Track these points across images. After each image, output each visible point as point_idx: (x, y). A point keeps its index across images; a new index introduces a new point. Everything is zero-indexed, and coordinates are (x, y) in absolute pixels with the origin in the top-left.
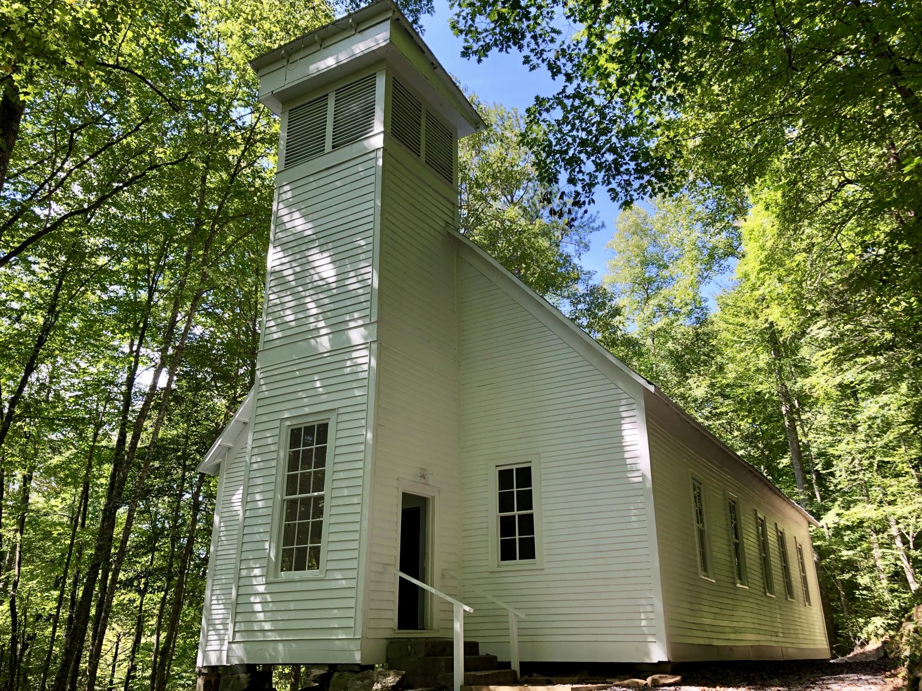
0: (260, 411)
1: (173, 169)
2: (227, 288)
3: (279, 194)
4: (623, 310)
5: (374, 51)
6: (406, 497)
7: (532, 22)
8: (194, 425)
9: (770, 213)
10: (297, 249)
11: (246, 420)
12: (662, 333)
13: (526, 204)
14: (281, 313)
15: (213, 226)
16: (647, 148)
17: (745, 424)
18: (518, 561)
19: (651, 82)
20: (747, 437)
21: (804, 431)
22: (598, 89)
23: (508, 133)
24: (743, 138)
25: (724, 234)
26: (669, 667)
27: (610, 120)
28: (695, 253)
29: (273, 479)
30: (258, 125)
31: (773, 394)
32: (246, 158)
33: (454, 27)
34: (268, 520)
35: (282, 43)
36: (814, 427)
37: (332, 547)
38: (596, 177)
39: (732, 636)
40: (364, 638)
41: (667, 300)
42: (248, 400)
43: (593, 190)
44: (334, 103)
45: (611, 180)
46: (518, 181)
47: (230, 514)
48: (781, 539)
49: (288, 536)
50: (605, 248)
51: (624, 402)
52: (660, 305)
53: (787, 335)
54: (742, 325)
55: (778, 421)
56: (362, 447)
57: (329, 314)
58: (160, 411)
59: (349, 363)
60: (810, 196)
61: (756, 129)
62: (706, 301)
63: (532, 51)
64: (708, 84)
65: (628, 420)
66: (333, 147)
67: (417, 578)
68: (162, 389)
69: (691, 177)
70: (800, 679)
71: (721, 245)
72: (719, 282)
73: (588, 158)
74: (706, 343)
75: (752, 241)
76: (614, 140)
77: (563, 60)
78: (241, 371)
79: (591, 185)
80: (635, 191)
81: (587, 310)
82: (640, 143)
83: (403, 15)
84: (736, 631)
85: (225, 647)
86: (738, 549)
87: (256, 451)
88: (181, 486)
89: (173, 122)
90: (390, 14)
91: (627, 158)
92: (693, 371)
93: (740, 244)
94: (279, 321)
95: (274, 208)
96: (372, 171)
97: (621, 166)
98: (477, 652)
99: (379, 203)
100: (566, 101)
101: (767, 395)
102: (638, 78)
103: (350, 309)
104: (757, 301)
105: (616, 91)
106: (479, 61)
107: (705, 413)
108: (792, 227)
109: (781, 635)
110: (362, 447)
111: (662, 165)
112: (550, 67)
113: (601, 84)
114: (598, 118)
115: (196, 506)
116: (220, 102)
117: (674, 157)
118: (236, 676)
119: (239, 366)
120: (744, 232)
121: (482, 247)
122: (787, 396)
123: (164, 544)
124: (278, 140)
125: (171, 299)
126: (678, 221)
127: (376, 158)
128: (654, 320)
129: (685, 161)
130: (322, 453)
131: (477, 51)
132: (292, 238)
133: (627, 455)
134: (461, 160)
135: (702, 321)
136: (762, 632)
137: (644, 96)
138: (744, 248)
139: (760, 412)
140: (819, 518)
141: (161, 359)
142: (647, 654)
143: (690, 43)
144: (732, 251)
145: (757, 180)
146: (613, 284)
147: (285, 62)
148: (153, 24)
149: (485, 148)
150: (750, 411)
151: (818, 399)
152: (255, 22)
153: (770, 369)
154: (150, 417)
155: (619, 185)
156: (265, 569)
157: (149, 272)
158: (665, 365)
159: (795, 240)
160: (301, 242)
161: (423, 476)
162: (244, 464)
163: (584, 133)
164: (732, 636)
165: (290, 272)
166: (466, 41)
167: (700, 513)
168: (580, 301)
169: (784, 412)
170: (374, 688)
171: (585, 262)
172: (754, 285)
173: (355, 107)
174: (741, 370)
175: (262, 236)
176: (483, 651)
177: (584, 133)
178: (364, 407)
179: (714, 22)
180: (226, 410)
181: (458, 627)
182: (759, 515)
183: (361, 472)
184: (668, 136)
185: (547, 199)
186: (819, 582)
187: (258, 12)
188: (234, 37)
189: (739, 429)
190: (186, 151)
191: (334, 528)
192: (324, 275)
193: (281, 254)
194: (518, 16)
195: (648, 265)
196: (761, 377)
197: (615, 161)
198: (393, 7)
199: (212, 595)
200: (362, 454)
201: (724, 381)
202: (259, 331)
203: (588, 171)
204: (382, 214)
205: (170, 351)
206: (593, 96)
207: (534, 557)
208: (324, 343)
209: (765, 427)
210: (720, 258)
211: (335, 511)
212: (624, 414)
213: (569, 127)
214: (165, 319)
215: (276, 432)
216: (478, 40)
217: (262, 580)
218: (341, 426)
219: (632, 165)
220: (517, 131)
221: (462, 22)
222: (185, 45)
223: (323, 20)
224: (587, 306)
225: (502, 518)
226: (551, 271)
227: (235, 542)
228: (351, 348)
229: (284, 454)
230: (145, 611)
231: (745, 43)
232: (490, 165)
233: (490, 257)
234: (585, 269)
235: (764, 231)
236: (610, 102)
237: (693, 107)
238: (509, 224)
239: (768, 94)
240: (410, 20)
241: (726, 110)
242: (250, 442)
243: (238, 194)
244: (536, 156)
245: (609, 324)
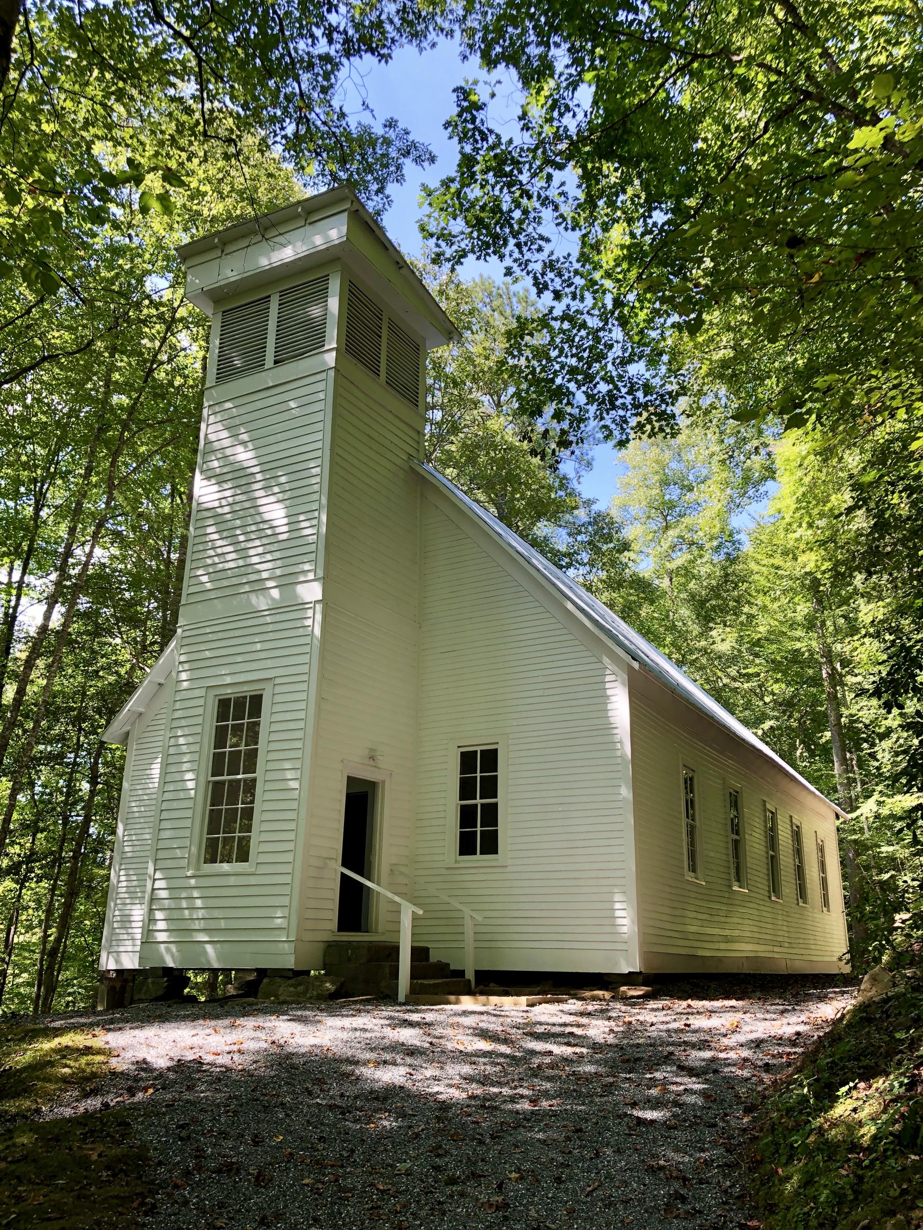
6: (351, 781)
18: (478, 856)
26: (641, 978)
33: (423, 229)
38: (587, 411)
39: (723, 946)
41: (690, 530)
44: (277, 303)
45: (605, 415)
48: (797, 835)
52: (682, 537)
54: (778, 568)
62: (738, 532)
63: (515, 261)
66: (276, 362)
67: (362, 875)
73: (579, 388)
76: (610, 367)
77: (551, 275)
79: (581, 420)
81: (590, 543)
84: (727, 940)
90: (347, 205)
91: (624, 390)
92: (718, 621)
97: (617, 399)
98: (427, 957)
100: (553, 323)
107: (733, 671)
135: (732, 560)
146: (624, 508)
155: (614, 421)
158: (685, 612)
161: (372, 758)
164: (723, 946)
166: (438, 246)
167: (690, 804)
171: (586, 487)
176: (434, 957)
178: (305, 678)
182: (768, 806)
191: (266, 816)
193: (216, 488)
197: (610, 391)
207: (496, 852)
211: (268, 796)
218: (278, 699)
219: (629, 398)
225: (463, 807)
236: (606, 323)
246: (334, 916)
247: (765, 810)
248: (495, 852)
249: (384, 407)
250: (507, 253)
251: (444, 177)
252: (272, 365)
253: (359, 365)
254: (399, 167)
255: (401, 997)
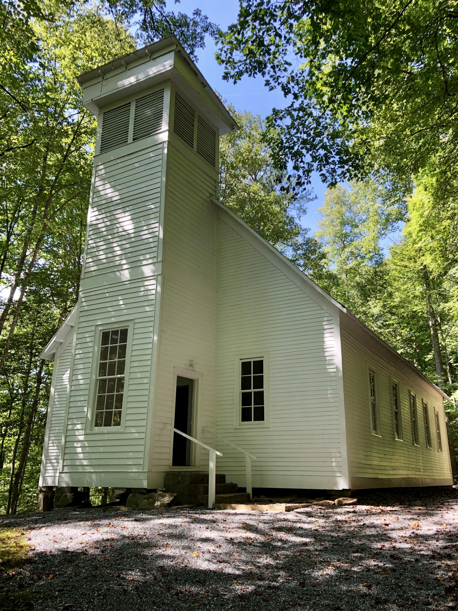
0: (82, 319)
1: (23, 151)
2: (60, 234)
3: (96, 171)
4: (327, 255)
5: (163, 73)
6: (180, 379)
7: (271, 57)
8: (38, 326)
9: (427, 192)
10: (107, 210)
11: (73, 325)
12: (353, 271)
13: (264, 181)
14: (97, 253)
15: (51, 191)
16: (347, 147)
17: (405, 332)
18: (253, 422)
19: (352, 101)
20: (406, 340)
21: (443, 337)
22: (316, 105)
23: (254, 133)
24: (412, 141)
25: (396, 206)
26: (350, 493)
27: (323, 127)
28: (377, 217)
29: (90, 365)
30: (83, 122)
31: (424, 313)
32: (74, 144)
33: (218, 58)
34: (87, 392)
35: (100, 65)
36: (450, 334)
37: (129, 411)
38: (313, 166)
39: (391, 472)
40: (149, 472)
41: (357, 248)
42: (74, 311)
43: (310, 174)
44: (135, 108)
45: (323, 168)
46: (260, 165)
47: (62, 387)
49: (100, 402)
50: (317, 212)
51: (325, 319)
53: (435, 274)
54: (406, 267)
55: (426, 331)
56: (150, 346)
57: (129, 255)
58: (15, 316)
59: (142, 289)
60: (455, 181)
61: (421, 135)
62: (382, 250)
63: (271, 76)
64: (390, 103)
65: (328, 331)
66: (134, 140)
67: (186, 433)
68: (17, 301)
69: (376, 167)
70: (434, 501)
71: (394, 213)
72: (392, 238)
73: (307, 153)
74: (382, 278)
75: (415, 211)
76: (325, 140)
77: (292, 84)
78: (71, 290)
79: (309, 171)
80: (338, 176)
81: (304, 254)
82: (343, 143)
83: (183, 48)
85: (58, 474)
86: (397, 415)
87: (79, 346)
88: (29, 366)
89: (24, 118)
91: (334, 153)
92: (372, 296)
93: (407, 212)
94: (95, 259)
95: (93, 180)
96: (160, 157)
97: (330, 159)
99: (164, 179)
100: (293, 113)
101: (420, 313)
102: (343, 98)
103: (144, 252)
104: (416, 251)
105: (328, 107)
106: (235, 83)
107: (379, 323)
108: (442, 202)
109: (422, 470)
110: (150, 346)
111: (357, 158)
112: (284, 88)
113: (317, 101)
114: (315, 125)
115: (39, 380)
116: (56, 105)
117: (365, 154)
118: (64, 494)
119: (68, 287)
120: (410, 207)
121: (235, 211)
122: (433, 314)
123: (17, 405)
124: (96, 132)
125: (22, 240)
126: (366, 196)
127: (163, 148)
128: (348, 262)
129: (372, 156)
130: (123, 349)
131: (233, 76)
132: (104, 202)
133: (326, 354)
134: (221, 150)
135: (379, 263)
136: (410, 469)
137: (346, 111)
138: (408, 215)
139: (415, 325)
140: (450, 395)
141: (16, 281)
142: (336, 484)
143: (379, 74)
144: (401, 217)
145: (420, 170)
146: (322, 237)
147: (100, 79)
148: (9, 48)
149: (238, 142)
150: (408, 324)
151: (453, 317)
152: (81, 49)
153: (423, 296)
154: (8, 320)
155: (328, 171)
156: (84, 425)
157: (7, 221)
158: (354, 292)
159: (443, 211)
160: (111, 204)
161: (191, 365)
162: (70, 354)
163: (305, 135)
164: (391, 472)
165: (103, 225)
166: (226, 68)
167: (373, 393)
168: (299, 248)
169: (431, 325)
170: (156, 504)
172: (415, 240)
173: (149, 112)
174: (404, 296)
175: (85, 199)
176: (228, 480)
177: (305, 135)
178: (152, 319)
179: (396, 60)
180: (59, 316)
181: (212, 465)
182: (412, 393)
183: (150, 362)
184: (362, 139)
185: (279, 180)
186: (448, 436)
187: (83, 42)
188: (66, 59)
189: (400, 335)
190: (33, 138)
192: (126, 228)
193: (97, 213)
194: (262, 51)
195: (345, 225)
196: (417, 302)
197: (325, 155)
198: (177, 43)
199: (49, 440)
200: (151, 350)
201: (392, 304)
202: (82, 263)
203: (306, 161)
204: (166, 188)
205: (22, 276)
206: (312, 110)
207: (263, 420)
208: (126, 275)
209: (417, 334)
210: (393, 221)
211: (131, 387)
212: (326, 327)
213: (295, 131)
214: (19, 254)
215: (93, 334)
216: (235, 68)
217: (82, 432)
218: (137, 331)
219: (337, 158)
220: (260, 131)
221: (224, 54)
222: (31, 64)
223: (129, 50)
224: (303, 252)
225: (243, 394)
226: (281, 227)
227: (65, 405)
228: (144, 278)
229: (98, 349)
230: (6, 447)
231: (416, 75)
232: (241, 154)
233: (239, 216)
234: (303, 227)
235: (423, 204)
237: (379, 119)
238: (253, 195)
239: (430, 111)
240: (188, 51)
241: (401, 122)
242: (75, 340)
243: (70, 170)
244: (272, 150)
245: (318, 264)
246: (170, 457)
247: (410, 395)
248: (263, 419)
249: (196, 166)
250: (267, 72)
251: (230, 25)
252: (132, 141)
253: (182, 140)
254: (202, 38)
255: (210, 505)
